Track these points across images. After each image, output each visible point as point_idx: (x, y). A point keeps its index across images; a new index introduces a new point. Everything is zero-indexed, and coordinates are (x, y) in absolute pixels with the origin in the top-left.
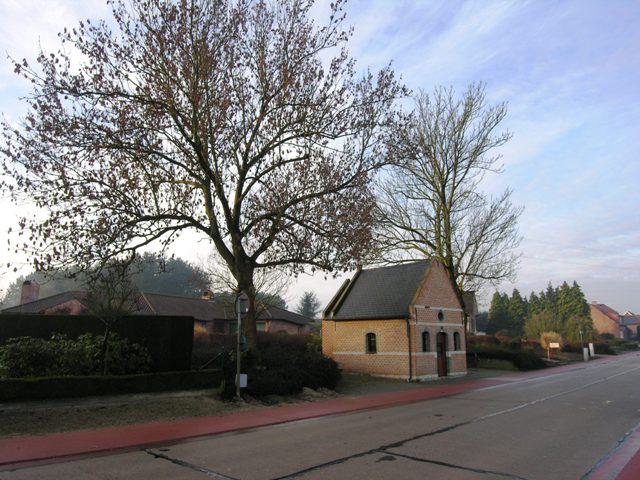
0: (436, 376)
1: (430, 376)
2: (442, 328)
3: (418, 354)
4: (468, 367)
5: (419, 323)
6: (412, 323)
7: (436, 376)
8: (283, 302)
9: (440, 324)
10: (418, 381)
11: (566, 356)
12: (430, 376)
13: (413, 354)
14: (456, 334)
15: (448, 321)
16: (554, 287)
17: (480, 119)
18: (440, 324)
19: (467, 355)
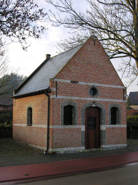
0: (82, 149)
1: (72, 149)
2: (94, 102)
3: (59, 127)
4: (129, 136)
5: (60, 97)
6: (52, 97)
7: (84, 148)
8: (13, 76)
9: (92, 99)
10: (54, 153)
11: (76, 80)
12: (72, 149)
13: (51, 127)
14: (114, 110)
15: (104, 97)
16: (26, 76)
17: (102, 33)
18: (92, 99)
19: (128, 128)
